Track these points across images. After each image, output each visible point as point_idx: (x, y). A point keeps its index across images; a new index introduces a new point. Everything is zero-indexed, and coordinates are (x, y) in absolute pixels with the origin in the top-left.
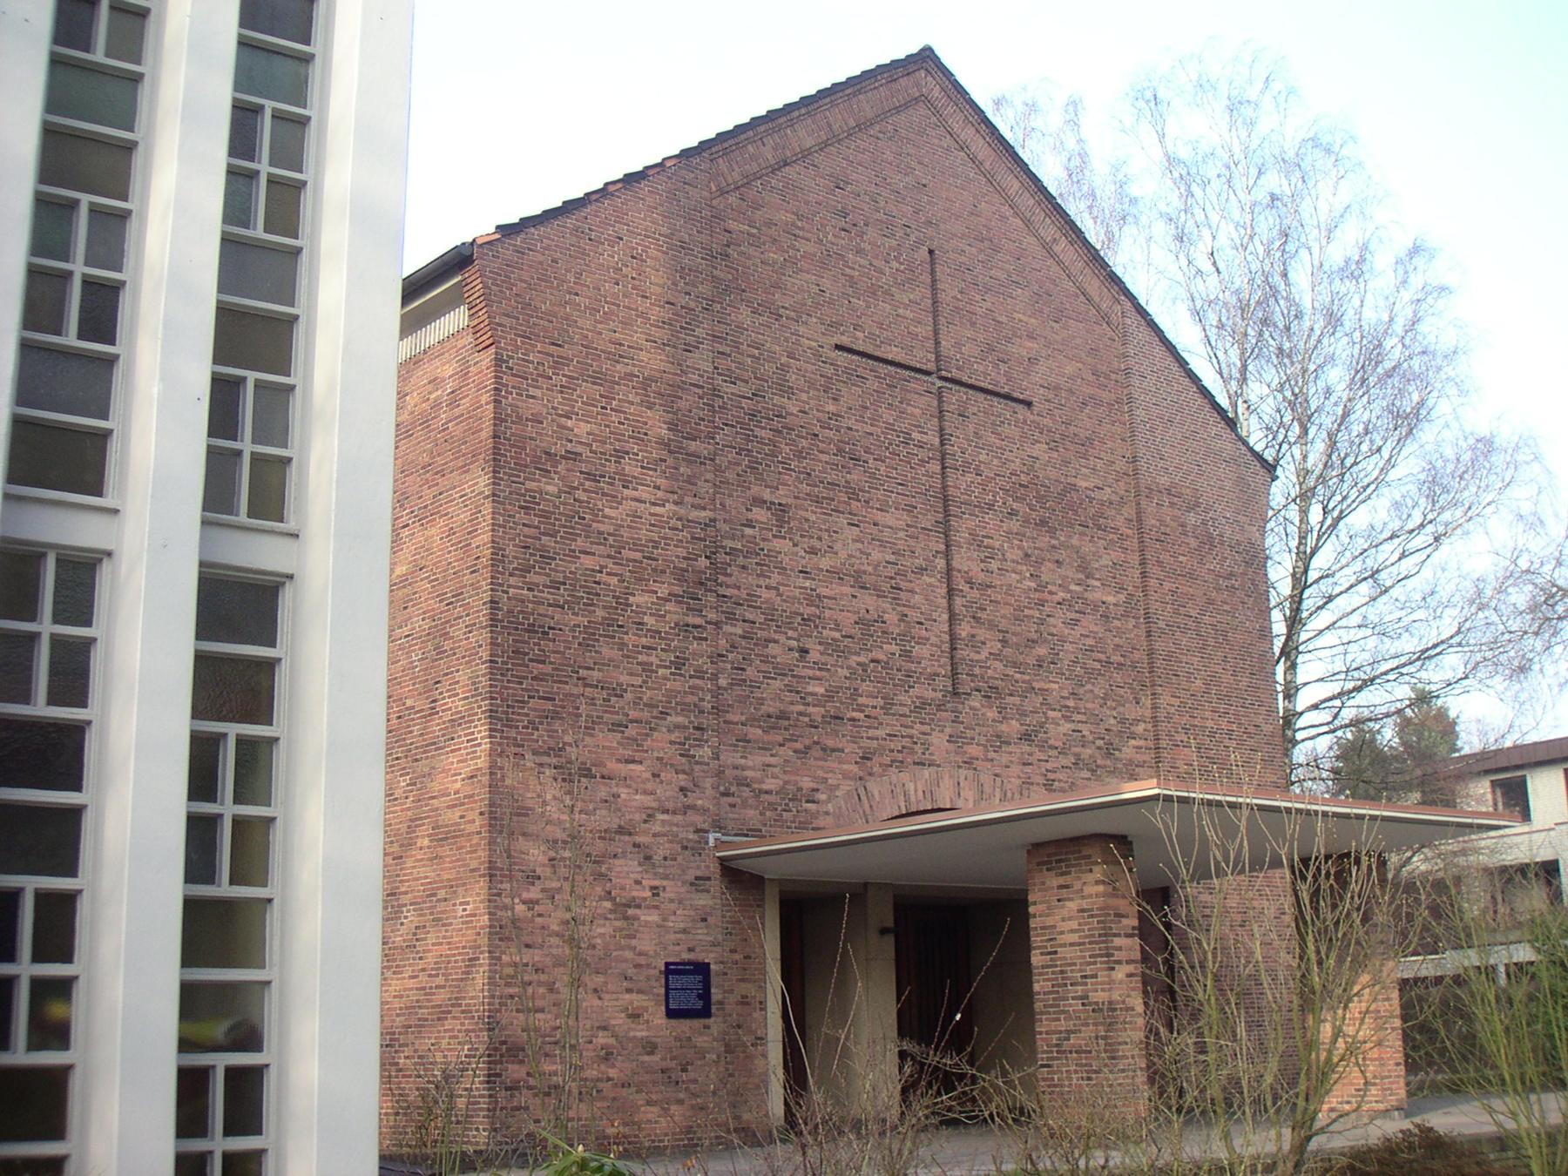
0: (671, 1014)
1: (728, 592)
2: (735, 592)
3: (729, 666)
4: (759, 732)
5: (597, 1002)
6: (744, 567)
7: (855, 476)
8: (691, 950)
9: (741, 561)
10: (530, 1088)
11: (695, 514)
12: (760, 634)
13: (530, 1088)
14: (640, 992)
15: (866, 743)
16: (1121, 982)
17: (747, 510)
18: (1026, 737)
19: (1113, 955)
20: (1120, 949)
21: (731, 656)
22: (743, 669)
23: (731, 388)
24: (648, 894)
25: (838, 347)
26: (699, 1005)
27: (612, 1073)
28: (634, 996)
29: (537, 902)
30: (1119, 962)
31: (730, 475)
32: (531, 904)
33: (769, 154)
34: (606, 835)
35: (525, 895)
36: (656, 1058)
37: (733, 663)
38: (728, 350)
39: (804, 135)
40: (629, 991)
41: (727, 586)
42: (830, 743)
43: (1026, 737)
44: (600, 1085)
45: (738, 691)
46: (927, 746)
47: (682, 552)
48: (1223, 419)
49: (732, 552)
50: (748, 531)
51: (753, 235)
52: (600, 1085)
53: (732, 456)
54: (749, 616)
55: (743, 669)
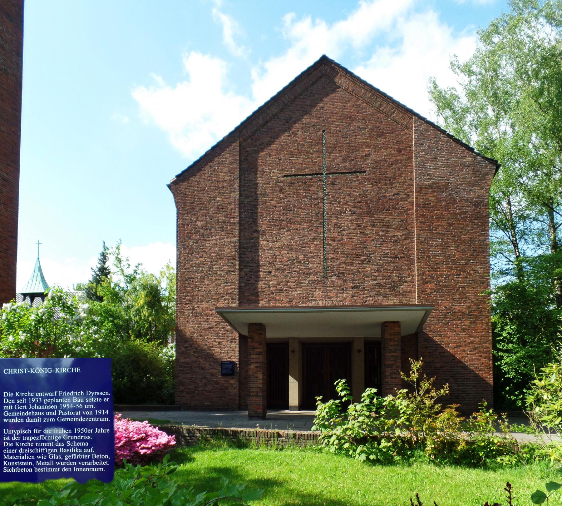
0: (223, 375)
1: (245, 259)
2: (248, 259)
3: (245, 280)
4: (254, 297)
5: (202, 372)
6: (250, 251)
7: (290, 216)
8: (230, 358)
9: (249, 250)
10: (185, 392)
11: (232, 240)
12: (255, 269)
13: (185, 392)
14: (215, 369)
15: (290, 296)
16: (253, 369)
17: (252, 234)
18: (354, 287)
19: (250, 361)
20: (254, 358)
21: (246, 277)
22: (249, 281)
23: (248, 200)
24: (217, 344)
25: (285, 176)
26: (231, 372)
27: (207, 389)
28: (213, 370)
29: (187, 347)
30: (253, 363)
31: (246, 226)
32: (186, 348)
33: (261, 121)
34: (206, 330)
35: (185, 346)
36: (218, 386)
37: (246, 279)
38: (246, 189)
39: (274, 110)
40: (212, 369)
41: (245, 258)
42: (277, 298)
43: (354, 287)
44: (203, 392)
45: (248, 287)
46: (313, 295)
47: (228, 251)
48: (467, 149)
49: (247, 248)
50: (252, 241)
51: (256, 150)
52: (203, 392)
53: (247, 220)
54: (251, 265)
55: (249, 281)
